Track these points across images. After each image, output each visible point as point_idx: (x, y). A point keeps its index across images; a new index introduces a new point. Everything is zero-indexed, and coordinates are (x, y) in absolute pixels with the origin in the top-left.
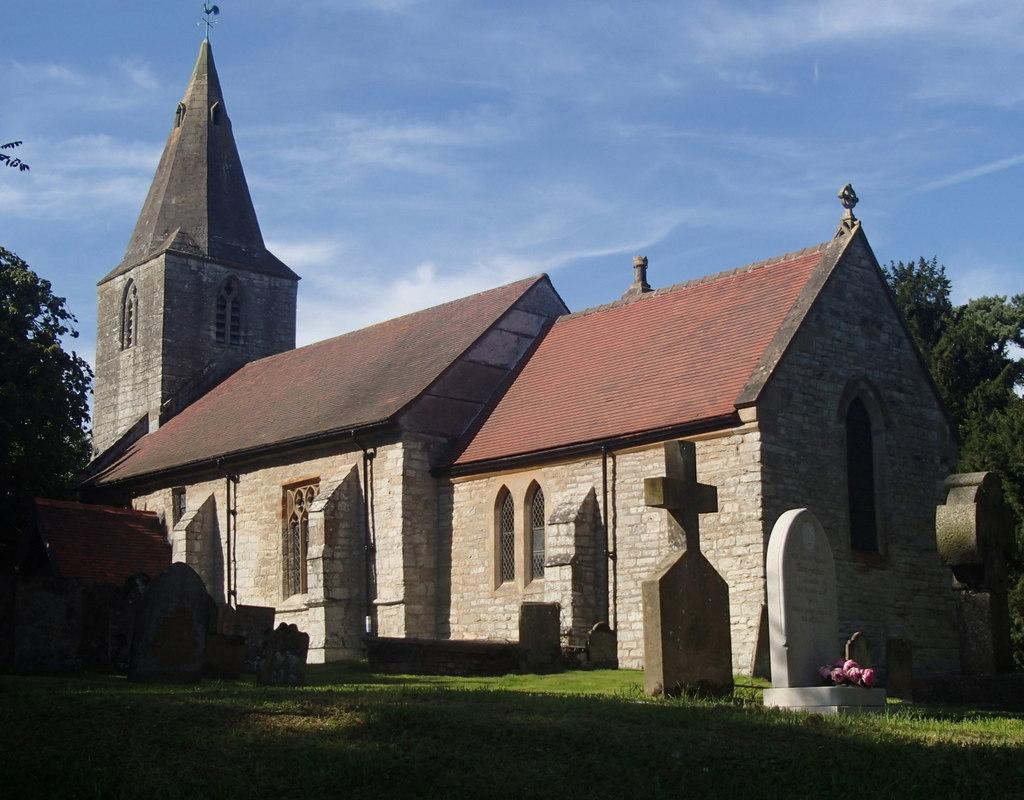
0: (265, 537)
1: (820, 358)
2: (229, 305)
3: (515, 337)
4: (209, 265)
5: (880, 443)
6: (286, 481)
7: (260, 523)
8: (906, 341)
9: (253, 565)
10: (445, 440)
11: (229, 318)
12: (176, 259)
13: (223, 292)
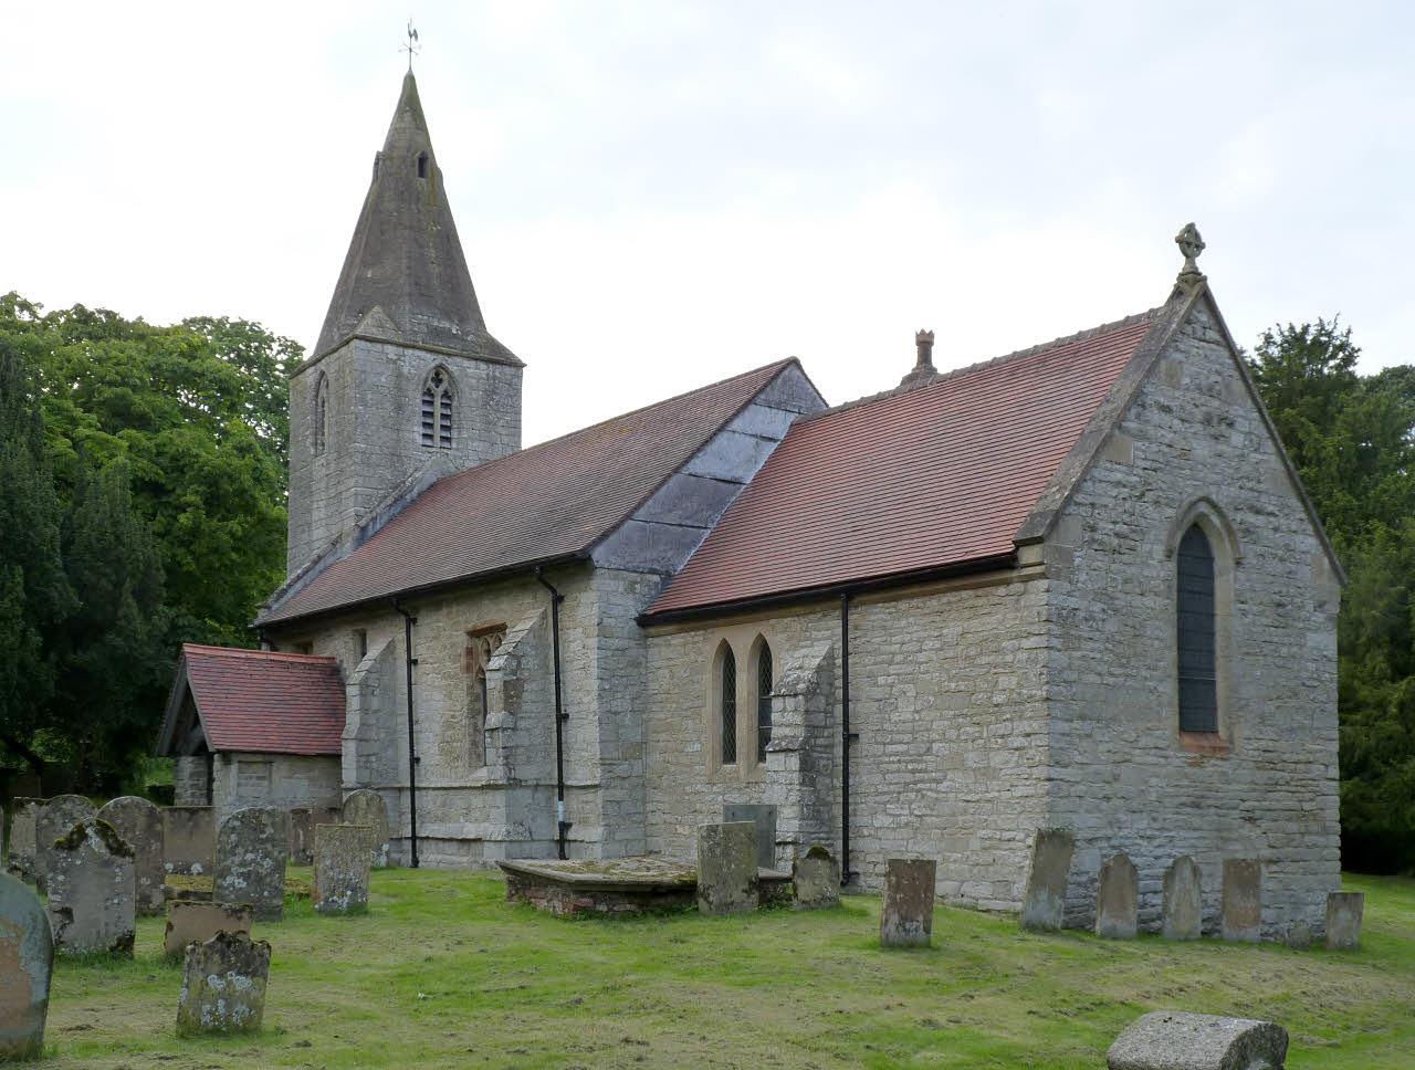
0: (449, 695)
1: (1141, 472)
2: (438, 401)
3: (754, 440)
4: (411, 351)
5: (1226, 585)
6: (470, 626)
7: (444, 677)
8: (1270, 443)
9: (437, 728)
10: (656, 578)
13: (431, 384)
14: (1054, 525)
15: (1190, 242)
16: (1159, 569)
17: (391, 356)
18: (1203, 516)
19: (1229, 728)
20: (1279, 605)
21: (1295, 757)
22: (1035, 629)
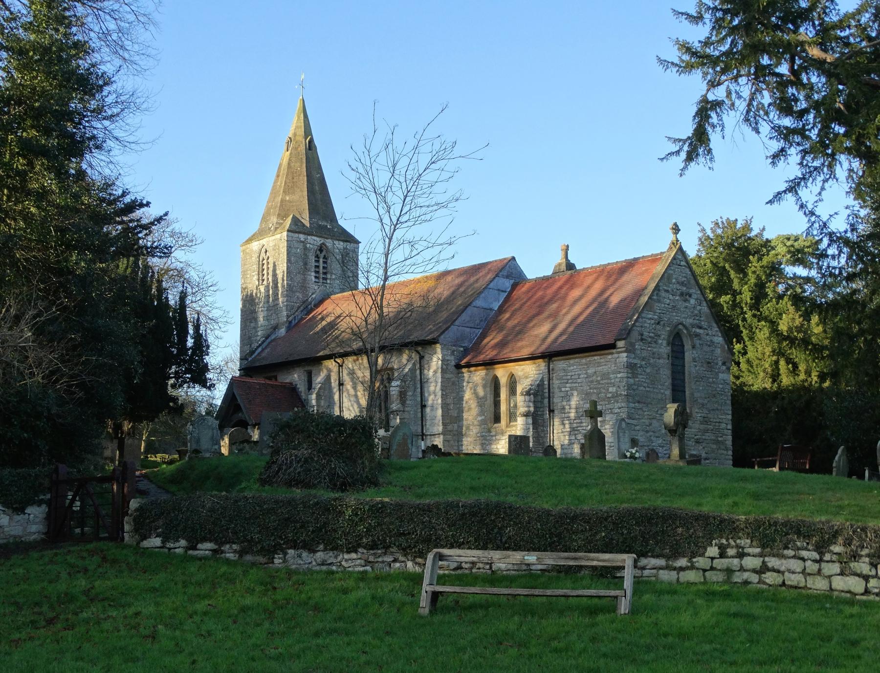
2: (321, 260)
5: (689, 355)
8: (704, 302)
11: (321, 268)
12: (293, 234)
13: (318, 252)
14: (629, 334)
15: (676, 229)
16: (664, 349)
17: (302, 239)
18: (680, 330)
19: (691, 408)
20: (709, 363)
21: (715, 420)
22: (622, 370)
